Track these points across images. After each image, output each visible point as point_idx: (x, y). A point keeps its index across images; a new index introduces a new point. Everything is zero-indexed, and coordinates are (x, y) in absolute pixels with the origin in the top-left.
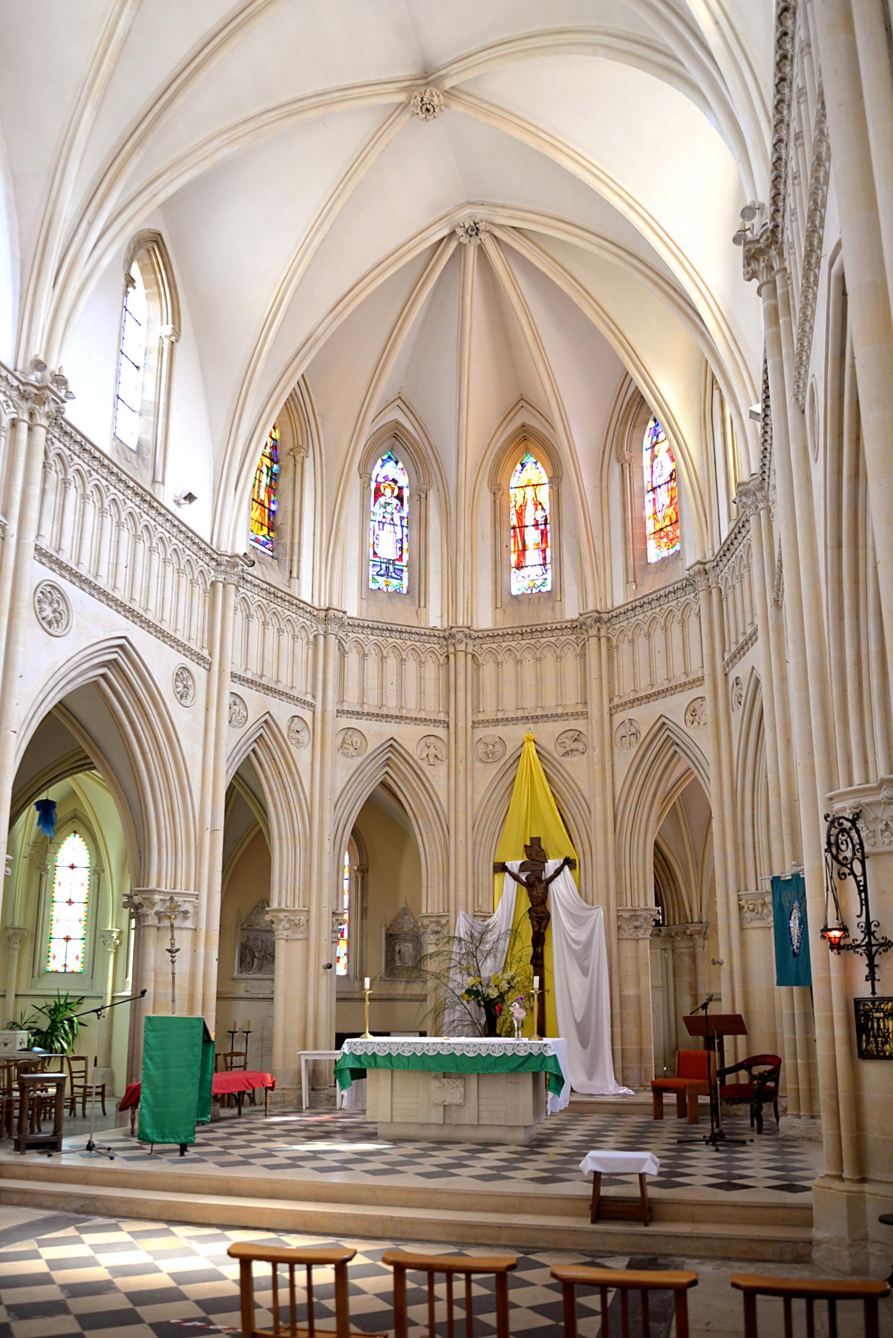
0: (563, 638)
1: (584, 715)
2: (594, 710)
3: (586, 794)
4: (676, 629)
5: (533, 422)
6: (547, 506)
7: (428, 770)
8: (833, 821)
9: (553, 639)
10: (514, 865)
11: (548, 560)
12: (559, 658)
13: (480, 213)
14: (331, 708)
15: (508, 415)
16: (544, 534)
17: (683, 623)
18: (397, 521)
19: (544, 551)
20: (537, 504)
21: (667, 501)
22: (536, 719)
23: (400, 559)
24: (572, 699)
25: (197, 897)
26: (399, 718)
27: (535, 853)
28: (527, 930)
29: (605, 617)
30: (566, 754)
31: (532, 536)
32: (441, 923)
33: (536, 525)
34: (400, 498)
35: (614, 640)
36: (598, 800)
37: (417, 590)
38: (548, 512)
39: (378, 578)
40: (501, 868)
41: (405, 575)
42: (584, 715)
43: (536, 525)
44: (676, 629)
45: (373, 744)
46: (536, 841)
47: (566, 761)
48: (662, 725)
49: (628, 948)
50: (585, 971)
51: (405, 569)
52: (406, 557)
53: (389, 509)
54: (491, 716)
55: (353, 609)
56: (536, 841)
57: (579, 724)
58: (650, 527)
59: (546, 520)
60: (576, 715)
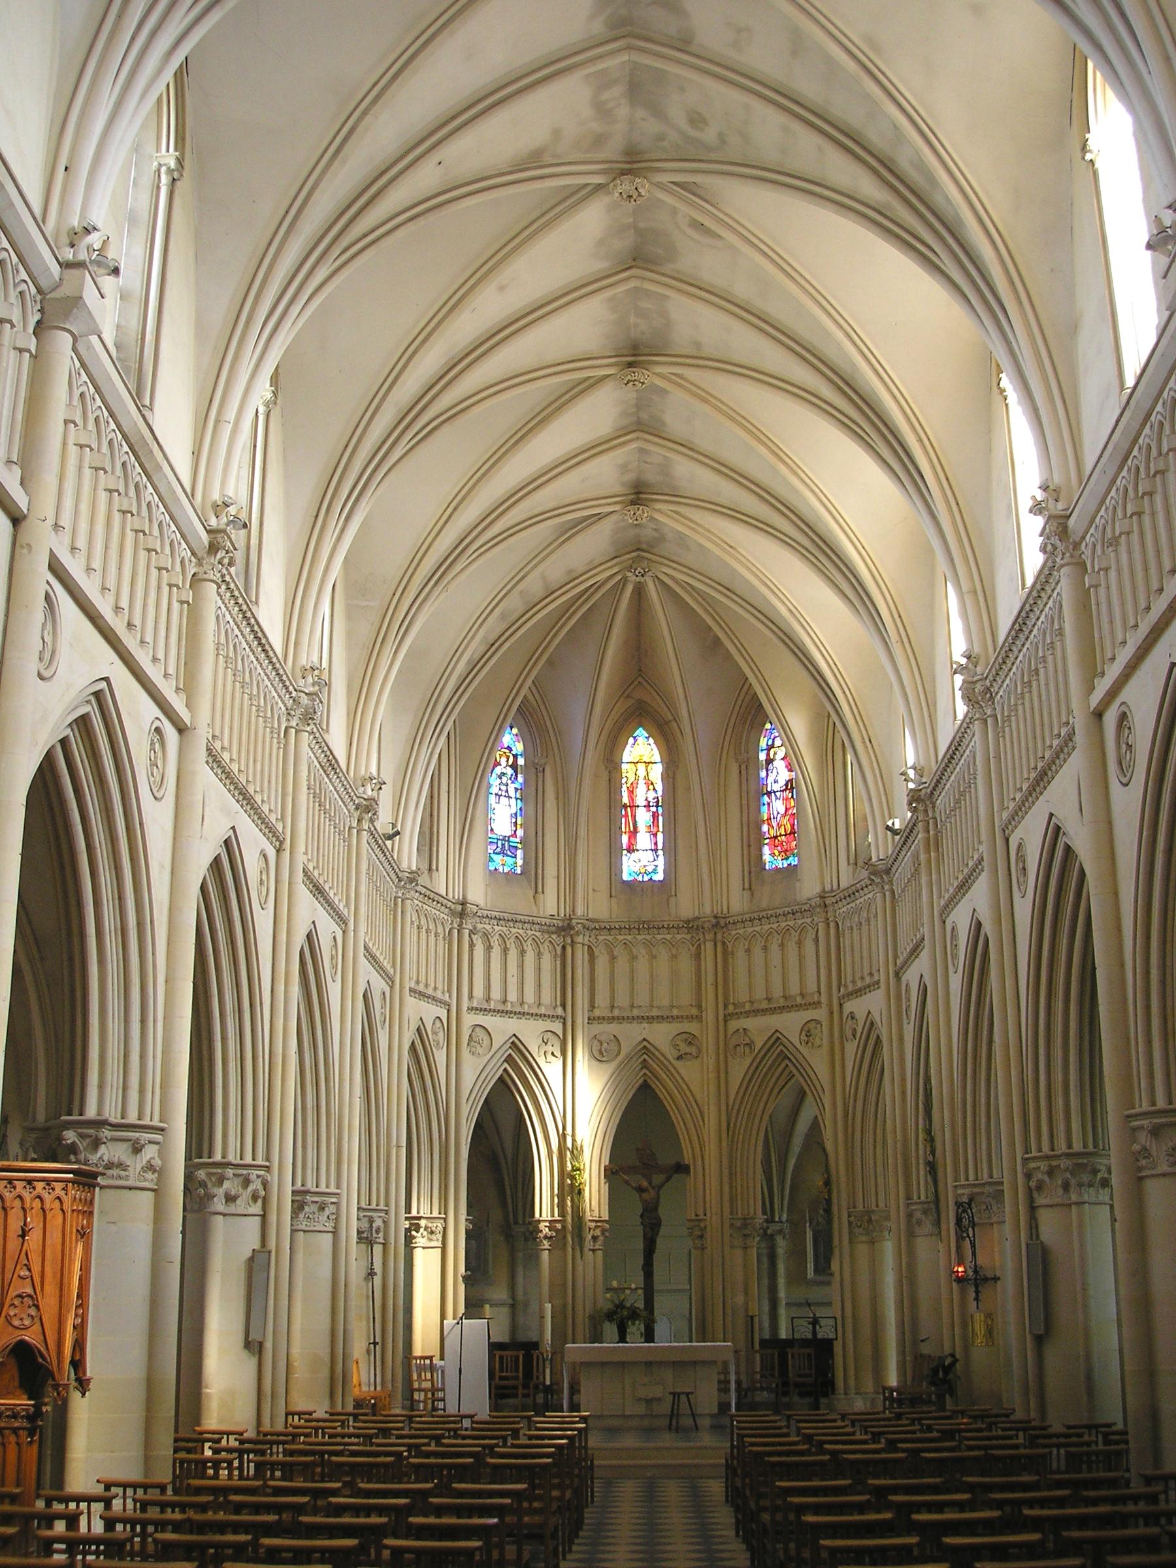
0: (678, 937)
1: (699, 1018)
2: (709, 1016)
3: (698, 1097)
4: (792, 948)
6: (659, 787)
8: (958, 1205)
9: (668, 937)
11: (660, 846)
12: (674, 957)
14: (465, 1004)
16: (655, 816)
17: (800, 943)
18: (512, 793)
19: (655, 835)
20: (649, 784)
21: (782, 811)
22: (651, 1019)
23: (515, 835)
24: (686, 997)
25: (387, 1212)
29: (722, 922)
30: (680, 1058)
31: (643, 817)
33: (648, 806)
34: (514, 766)
35: (730, 946)
36: (713, 1109)
37: (533, 873)
38: (660, 793)
39: (494, 857)
41: (519, 853)
43: (648, 806)
44: (792, 948)
45: (498, 1040)
51: (519, 846)
52: (520, 832)
53: (504, 780)
55: (477, 894)
57: (692, 1027)
59: (658, 802)
60: (690, 1018)
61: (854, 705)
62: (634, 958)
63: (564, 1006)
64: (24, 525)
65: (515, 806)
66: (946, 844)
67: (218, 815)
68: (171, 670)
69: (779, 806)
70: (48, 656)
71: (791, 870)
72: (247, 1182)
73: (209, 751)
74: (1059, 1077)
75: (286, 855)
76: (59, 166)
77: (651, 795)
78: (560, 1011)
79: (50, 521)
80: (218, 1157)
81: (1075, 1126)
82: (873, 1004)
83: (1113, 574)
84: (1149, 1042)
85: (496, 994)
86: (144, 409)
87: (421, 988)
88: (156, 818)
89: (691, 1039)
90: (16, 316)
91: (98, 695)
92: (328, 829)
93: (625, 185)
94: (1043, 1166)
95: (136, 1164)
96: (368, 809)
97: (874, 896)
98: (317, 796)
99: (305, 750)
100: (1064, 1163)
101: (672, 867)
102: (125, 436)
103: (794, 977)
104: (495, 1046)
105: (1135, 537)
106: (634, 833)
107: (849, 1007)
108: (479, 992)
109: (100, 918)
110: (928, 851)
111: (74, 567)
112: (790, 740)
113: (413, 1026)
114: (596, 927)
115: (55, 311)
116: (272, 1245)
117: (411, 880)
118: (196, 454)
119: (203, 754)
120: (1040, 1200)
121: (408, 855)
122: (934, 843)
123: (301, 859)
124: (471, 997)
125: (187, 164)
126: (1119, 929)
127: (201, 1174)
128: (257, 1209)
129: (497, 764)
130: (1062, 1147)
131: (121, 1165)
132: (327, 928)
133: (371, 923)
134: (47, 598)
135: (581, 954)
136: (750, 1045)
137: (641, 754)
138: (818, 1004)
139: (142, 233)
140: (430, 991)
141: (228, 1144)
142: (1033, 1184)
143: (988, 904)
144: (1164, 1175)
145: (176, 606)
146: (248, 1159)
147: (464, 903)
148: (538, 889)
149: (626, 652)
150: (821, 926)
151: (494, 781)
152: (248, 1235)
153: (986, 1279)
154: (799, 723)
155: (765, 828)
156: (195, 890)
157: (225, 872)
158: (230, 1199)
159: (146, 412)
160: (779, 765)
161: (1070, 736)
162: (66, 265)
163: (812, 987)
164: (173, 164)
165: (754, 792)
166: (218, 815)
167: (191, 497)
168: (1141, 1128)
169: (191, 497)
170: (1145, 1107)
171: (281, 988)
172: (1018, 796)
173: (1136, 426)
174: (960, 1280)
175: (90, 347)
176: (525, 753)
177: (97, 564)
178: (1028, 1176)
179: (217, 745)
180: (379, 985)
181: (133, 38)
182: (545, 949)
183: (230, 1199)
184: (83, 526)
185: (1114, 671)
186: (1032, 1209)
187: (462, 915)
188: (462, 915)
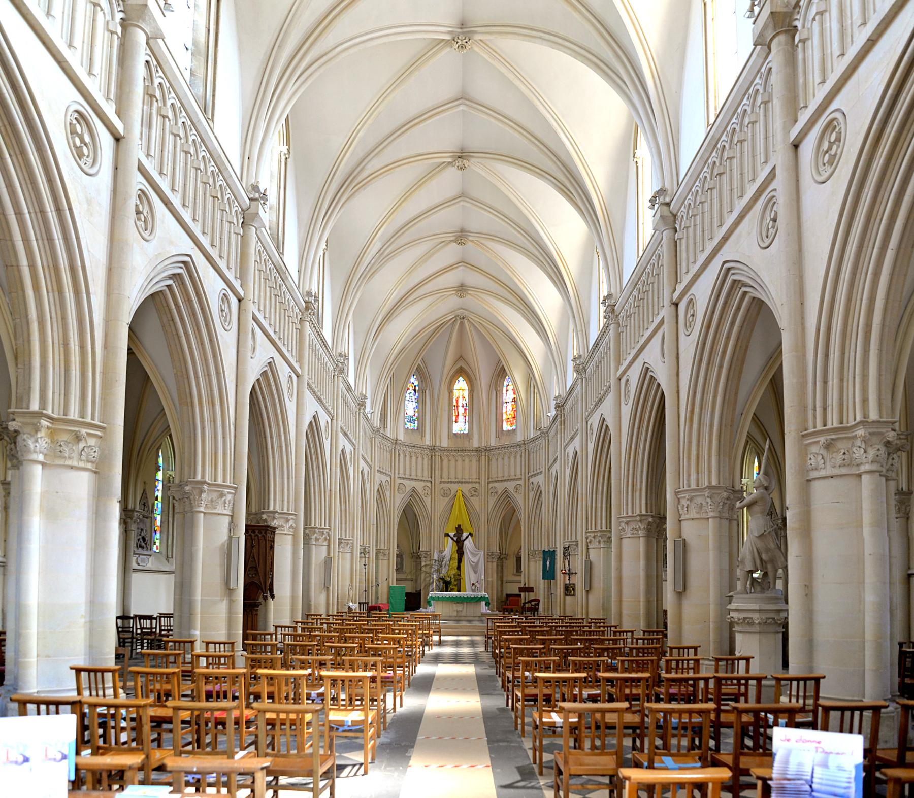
1: (479, 483)
4: (512, 459)
5: (465, 366)
6: (467, 399)
10: (452, 534)
13: (466, 313)
14: (397, 476)
17: (515, 457)
20: (463, 398)
22: (462, 483)
24: (474, 476)
27: (459, 530)
28: (456, 556)
31: (461, 410)
32: (428, 555)
34: (415, 390)
40: (447, 535)
44: (512, 459)
46: (459, 526)
48: (506, 491)
49: (490, 564)
50: (475, 572)
54: (446, 480)
55: (401, 437)
56: (459, 526)
57: (477, 486)
58: (505, 417)
60: (476, 483)
61: (229, 591)
62: (456, 461)
64: (242, 302)
65: (415, 405)
71: (514, 430)
76: (246, 158)
77: (464, 402)
81: (604, 522)
82: (540, 479)
85: (407, 472)
86: (281, 254)
88: (291, 407)
91: (269, 363)
92: (348, 412)
93: (459, 163)
94: (592, 535)
98: (345, 400)
99: (341, 385)
100: (599, 534)
101: (471, 428)
103: (512, 469)
107: (531, 480)
108: (401, 471)
109: (272, 443)
111: (260, 317)
112: (515, 383)
114: (443, 450)
115: (248, 219)
120: (590, 546)
121: (377, 423)
122: (563, 423)
123: (340, 423)
125: (291, 151)
126: (620, 455)
130: (599, 528)
132: (349, 448)
133: (363, 447)
135: (438, 459)
137: (461, 387)
139: (203, 59)
141: (316, 522)
148: (423, 435)
151: (407, 395)
158: (317, 539)
160: (510, 392)
163: (518, 473)
164: (286, 152)
165: (499, 404)
166: (311, 407)
167: (298, 288)
175: (261, 232)
178: (587, 538)
180: (366, 469)
184: (262, 301)
185: (626, 363)
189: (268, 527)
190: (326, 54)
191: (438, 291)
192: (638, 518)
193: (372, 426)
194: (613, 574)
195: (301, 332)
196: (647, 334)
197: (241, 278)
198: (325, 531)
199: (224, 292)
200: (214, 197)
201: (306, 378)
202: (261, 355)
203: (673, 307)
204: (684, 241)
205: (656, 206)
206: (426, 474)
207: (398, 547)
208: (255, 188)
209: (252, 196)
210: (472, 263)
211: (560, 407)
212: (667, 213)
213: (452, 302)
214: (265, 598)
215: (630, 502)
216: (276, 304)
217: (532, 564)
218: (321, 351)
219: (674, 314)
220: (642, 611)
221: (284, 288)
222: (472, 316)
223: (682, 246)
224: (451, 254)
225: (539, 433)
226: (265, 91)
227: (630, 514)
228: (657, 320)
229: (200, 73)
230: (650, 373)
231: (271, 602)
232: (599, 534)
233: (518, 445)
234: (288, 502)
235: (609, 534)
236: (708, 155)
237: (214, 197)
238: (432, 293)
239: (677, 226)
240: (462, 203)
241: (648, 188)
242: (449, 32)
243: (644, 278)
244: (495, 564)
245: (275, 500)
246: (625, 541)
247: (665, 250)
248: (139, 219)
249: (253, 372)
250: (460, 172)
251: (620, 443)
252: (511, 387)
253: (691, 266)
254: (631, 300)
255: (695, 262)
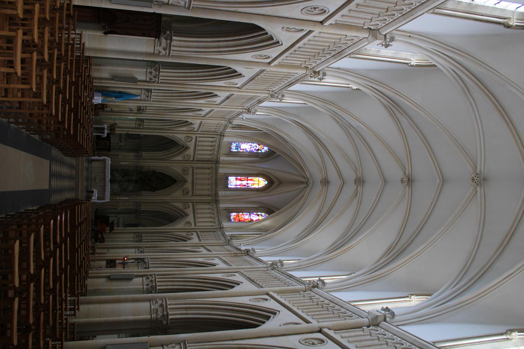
1: (193, 195)
6: (252, 187)
7: (181, 156)
8: (144, 259)
13: (310, 185)
15: (277, 179)
16: (245, 186)
20: (253, 184)
22: (193, 183)
25: (158, 83)
26: (195, 150)
30: (183, 190)
31: (244, 183)
34: (258, 150)
41: (236, 150)
42: (193, 195)
43: (247, 184)
45: (188, 144)
47: (181, 190)
48: (186, 215)
54: (195, 171)
55: (226, 139)
57: (190, 194)
60: (193, 193)
63: (197, 161)
65: (248, 150)
66: (236, 259)
67: (248, 72)
68: (284, 61)
69: (247, 217)
70: (288, 30)
71: (230, 220)
72: (155, 77)
73: (264, 70)
74: (176, 283)
75: (237, 90)
76: (410, 35)
77: (250, 185)
78: (195, 160)
79: (321, 31)
80: (161, 70)
83: (303, 298)
84: (185, 304)
85: (200, 143)
87: (202, 124)
88: (248, 56)
89: (187, 193)
90: (372, 23)
91: (278, 42)
93: (405, 179)
94: (153, 279)
95: (161, 49)
96: (248, 111)
97: (222, 241)
98: (251, 98)
99: (264, 95)
100: (154, 284)
101: (232, 189)
102: (343, 50)
104: (187, 143)
105: (312, 304)
106: (240, 180)
107: (195, 233)
108: (201, 139)
109: (222, 42)
110: (234, 254)
111: (310, 37)
113: (193, 122)
114: (216, 170)
115: (374, 32)
116: (139, 83)
117: (230, 122)
118: (339, 68)
119: (263, 69)
120: (144, 278)
121: (236, 122)
122: (236, 255)
123: (236, 93)
124: (200, 137)
125: (412, 67)
127: (157, 66)
128: (148, 79)
129: (259, 145)
131: (160, 45)
132: (218, 100)
134: (303, 30)
136: (185, 208)
137: (260, 182)
138: (195, 226)
139: (467, 10)
140: (201, 127)
141: (165, 73)
142: (149, 276)
143: (220, 267)
144: (151, 307)
145: (300, 62)
146: (160, 78)
147: (223, 136)
149: (288, 181)
150: (215, 227)
151: (255, 145)
152: (141, 77)
153: (124, 265)
154: (267, 223)
155: (241, 214)
156: (229, 66)
157: (233, 74)
158: (151, 73)
159: (349, 56)
160: (257, 218)
161: (262, 287)
162: (385, 36)
163: (200, 224)
164: (412, 64)
165: (250, 211)
166: (248, 72)
167: (327, 67)
168: (163, 301)
169: (327, 67)
170: (168, 303)
171: (204, 87)
172: (248, 275)
173: (340, 304)
174: (124, 258)
175: (365, 42)
176: (261, 153)
177: (311, 42)
178: (151, 275)
179: (265, 72)
180: (203, 113)
181: (443, 53)
182: (211, 156)
183: (151, 73)
184: (320, 39)
185: (278, 297)
186: (142, 276)
187: (221, 135)
188: (221, 135)
189: (160, 33)
190: (469, 92)
191: (325, 167)
192: (165, 313)
193: (233, 118)
194: (122, 296)
195: (299, 67)
196: (299, 312)
197: (336, 24)
198: (157, 79)
199: (327, 12)
200: (387, 9)
201: (268, 69)
202: (284, 36)
203: (319, 329)
204: (362, 333)
205: (383, 312)
206: (199, 157)
207: (146, 136)
208: (392, 39)
209: (388, 36)
210: (344, 189)
211: (247, 252)
212: (379, 319)
213: (318, 176)
214: (104, 27)
215: (177, 306)
216: (318, 49)
217: (132, 235)
218: (283, 84)
219: (313, 330)
220: (92, 320)
221: (328, 56)
222: (308, 190)
223: (359, 332)
224: (349, 174)
225: (229, 238)
226: (448, 50)
227: (169, 307)
228: (309, 318)
229: (460, 8)
230: (272, 316)
231: (100, 34)
232: (154, 284)
233: (220, 223)
234: (179, 51)
235: (154, 292)
236: (417, 345)
237: (379, 15)
238: (323, 162)
239: (371, 328)
240: (381, 182)
241: (392, 305)
242: (481, 171)
243: (337, 307)
244: (132, 207)
245: (180, 41)
246: (148, 304)
247: (357, 320)
248: (311, 8)
249: (273, 29)
250: (400, 179)
251: (222, 297)
252: (260, 218)
253: (346, 339)
254: (322, 299)
255: (349, 342)
